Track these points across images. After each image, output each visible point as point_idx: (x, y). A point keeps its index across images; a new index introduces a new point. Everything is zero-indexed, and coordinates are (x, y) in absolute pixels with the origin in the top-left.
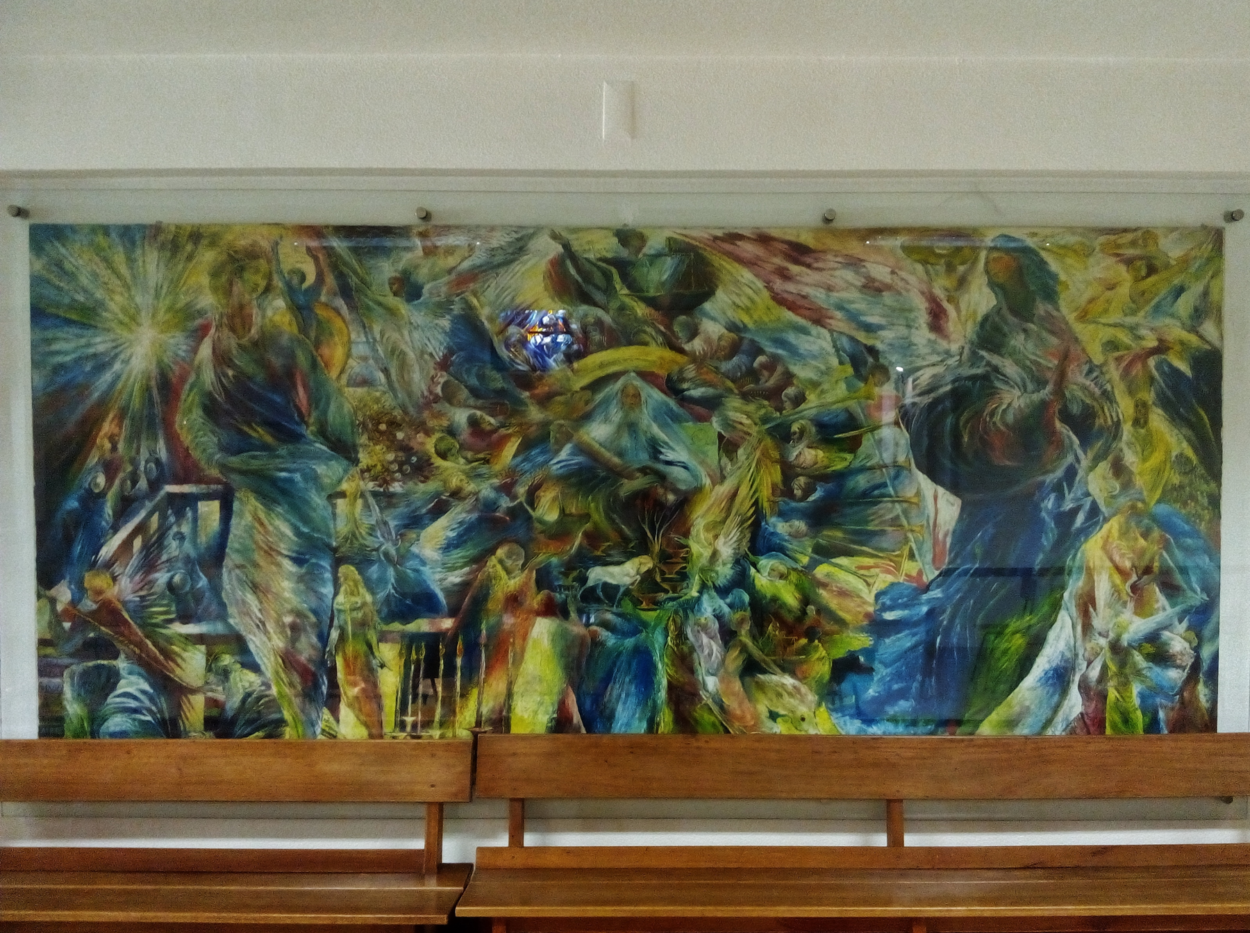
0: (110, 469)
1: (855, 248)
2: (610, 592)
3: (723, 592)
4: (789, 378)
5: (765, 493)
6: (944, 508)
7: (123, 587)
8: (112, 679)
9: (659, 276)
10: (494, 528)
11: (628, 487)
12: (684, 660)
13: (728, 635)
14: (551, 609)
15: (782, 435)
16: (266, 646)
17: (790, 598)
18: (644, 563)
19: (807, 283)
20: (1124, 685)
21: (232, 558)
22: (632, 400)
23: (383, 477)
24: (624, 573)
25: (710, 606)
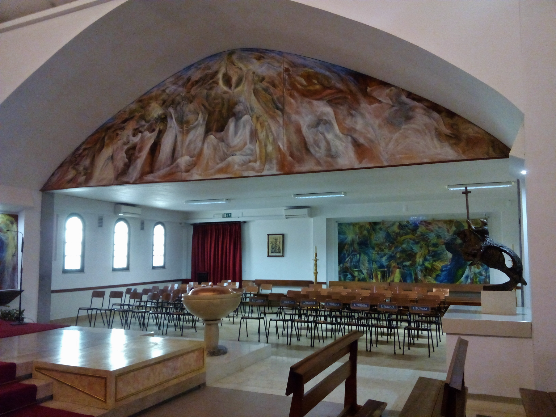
0: (347, 251)
1: (437, 223)
2: (406, 266)
3: (421, 266)
4: (429, 239)
5: (426, 253)
6: (450, 255)
7: (348, 265)
8: (347, 275)
9: (411, 227)
10: (391, 258)
11: (408, 252)
12: (416, 274)
13: (422, 271)
14: (398, 268)
15: (428, 246)
16: (365, 272)
17: (430, 267)
18: (411, 262)
19: (431, 227)
20: (476, 279)
21: (361, 261)
22: (408, 242)
23: (378, 252)
24: (408, 263)
25: (419, 268)
